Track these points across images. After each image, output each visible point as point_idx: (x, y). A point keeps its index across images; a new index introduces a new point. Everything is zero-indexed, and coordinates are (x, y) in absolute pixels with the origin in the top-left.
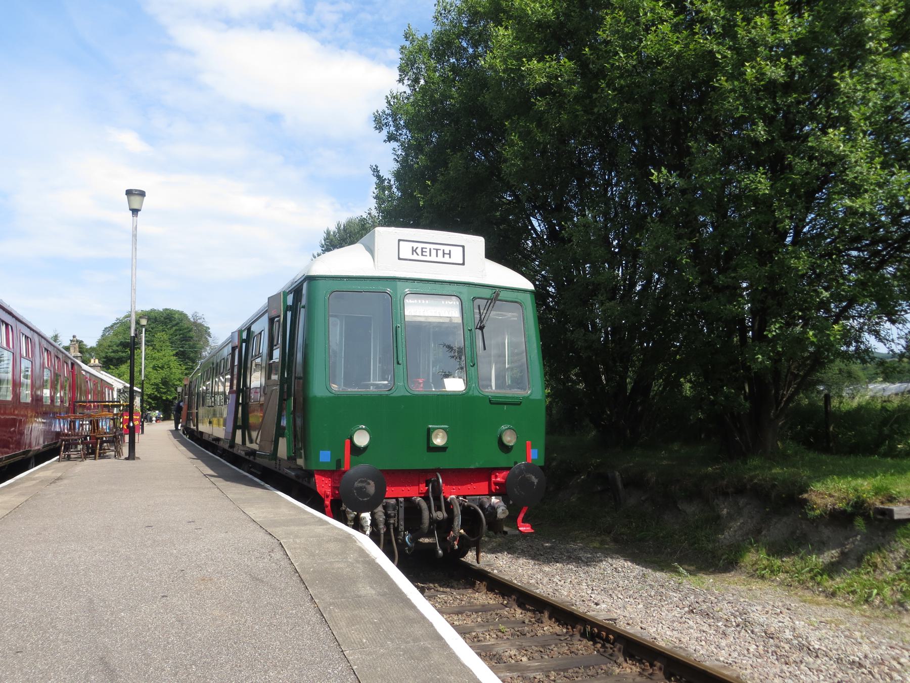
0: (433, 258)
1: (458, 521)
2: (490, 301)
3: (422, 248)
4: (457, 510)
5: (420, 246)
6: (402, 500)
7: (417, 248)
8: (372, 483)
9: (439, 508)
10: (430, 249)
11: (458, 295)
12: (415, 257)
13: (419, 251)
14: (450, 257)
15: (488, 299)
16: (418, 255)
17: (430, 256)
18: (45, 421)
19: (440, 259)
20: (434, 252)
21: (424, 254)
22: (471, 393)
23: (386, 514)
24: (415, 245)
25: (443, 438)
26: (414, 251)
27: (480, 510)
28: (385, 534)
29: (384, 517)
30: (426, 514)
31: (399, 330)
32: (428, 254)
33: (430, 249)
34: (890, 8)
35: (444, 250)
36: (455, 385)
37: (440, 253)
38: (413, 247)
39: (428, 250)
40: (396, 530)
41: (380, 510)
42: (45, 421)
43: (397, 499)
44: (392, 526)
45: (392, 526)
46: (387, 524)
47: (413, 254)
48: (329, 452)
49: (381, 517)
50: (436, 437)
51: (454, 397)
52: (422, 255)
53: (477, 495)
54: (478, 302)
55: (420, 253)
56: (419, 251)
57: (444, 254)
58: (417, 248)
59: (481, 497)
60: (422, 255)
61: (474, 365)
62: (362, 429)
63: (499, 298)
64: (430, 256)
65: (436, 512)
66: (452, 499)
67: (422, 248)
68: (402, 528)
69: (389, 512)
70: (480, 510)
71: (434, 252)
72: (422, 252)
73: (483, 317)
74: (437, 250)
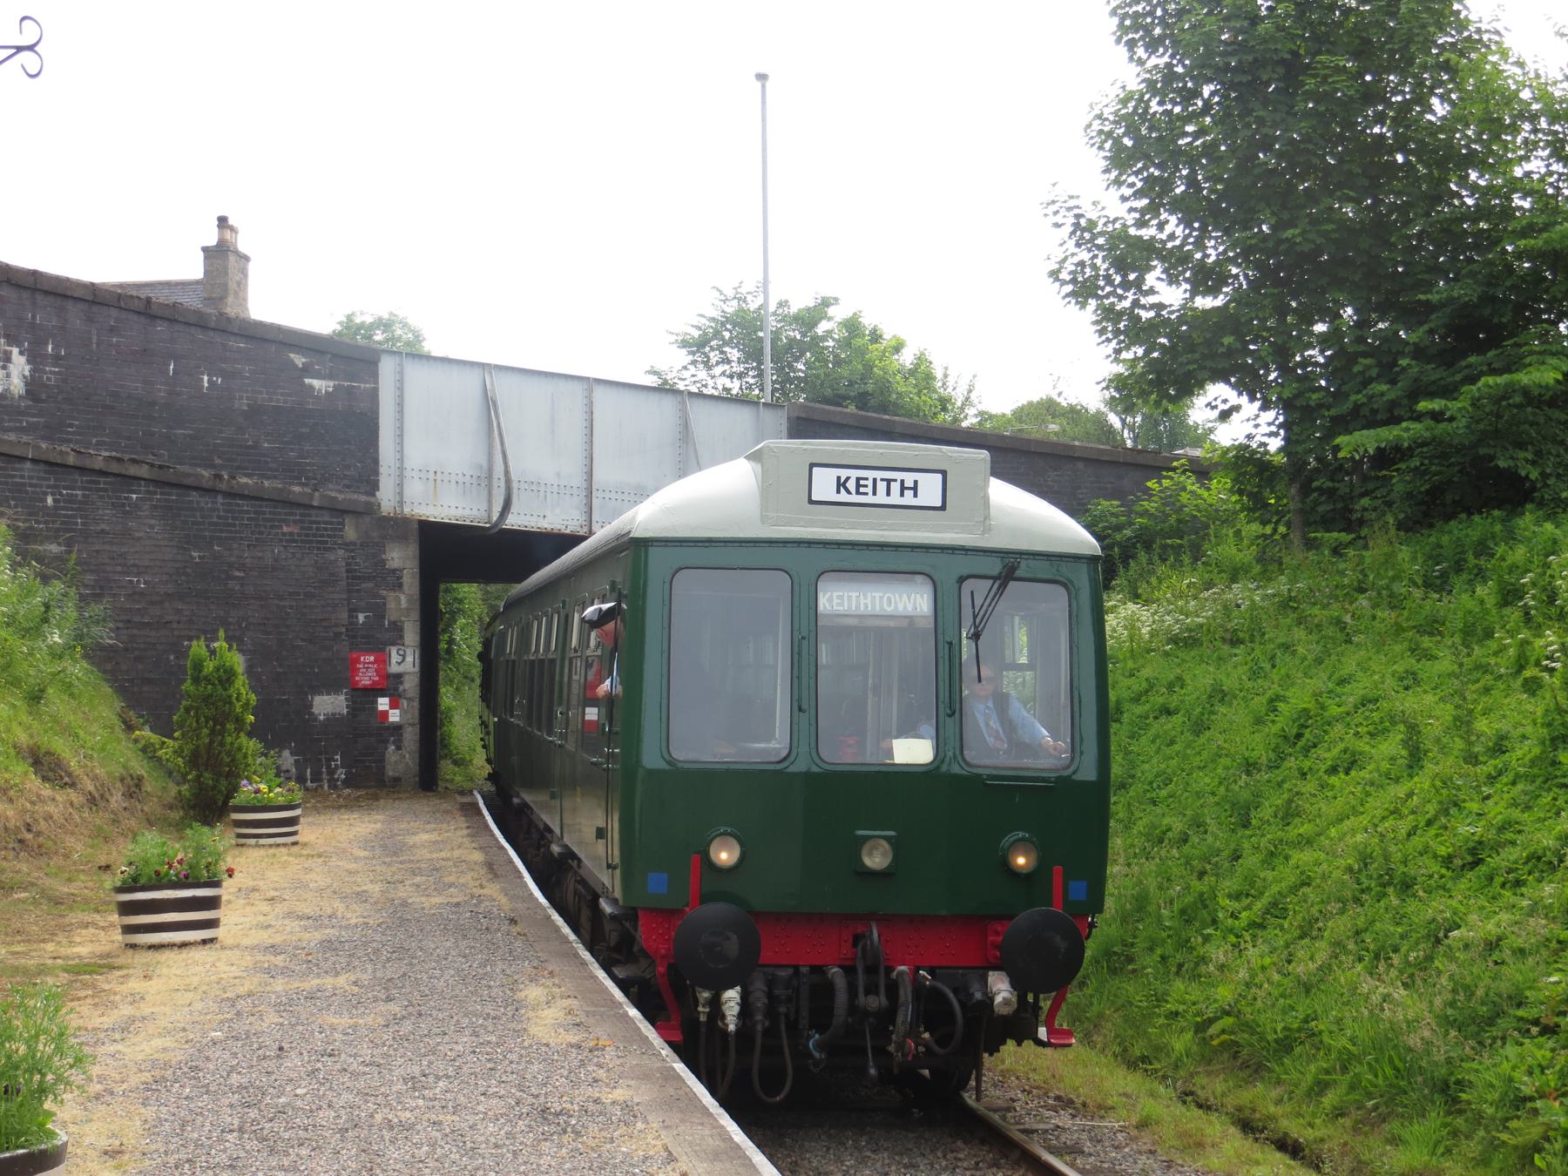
0: (881, 498)
1: (905, 1015)
2: (998, 583)
3: (858, 479)
4: (905, 994)
5: (855, 474)
6: (804, 970)
7: (848, 478)
8: (734, 938)
9: (871, 990)
10: (875, 480)
11: (927, 570)
12: (843, 497)
13: (851, 485)
14: (915, 495)
15: (995, 578)
16: (849, 492)
17: (874, 493)
18: (1385, 399)
19: (895, 498)
20: (882, 486)
21: (862, 490)
22: (944, 768)
23: (770, 995)
24: (844, 473)
25: (884, 854)
26: (841, 485)
27: (951, 996)
28: (766, 1032)
29: (766, 1001)
30: (841, 998)
31: (805, 643)
32: (869, 490)
33: (875, 480)
34: (49, 647)
35: (902, 482)
36: (913, 751)
37: (896, 487)
38: (839, 478)
39: (870, 483)
40: (793, 1026)
41: (759, 985)
42: (1385, 399)
43: (796, 968)
44: (783, 1019)
45: (783, 1019)
46: (771, 1012)
47: (838, 491)
48: (666, 875)
49: (760, 1001)
50: (870, 854)
51: (909, 775)
52: (858, 492)
53: (959, 968)
54: (968, 586)
55: (853, 490)
56: (851, 485)
57: (903, 488)
58: (848, 478)
59: (967, 971)
60: (858, 492)
61: (954, 713)
62: (725, 834)
63: (1018, 573)
64: (874, 493)
65: (866, 995)
66: (901, 974)
67: (858, 479)
68: (804, 1023)
69: (776, 992)
70: (951, 996)
71: (882, 486)
72: (858, 486)
73: (978, 621)
74: (889, 481)
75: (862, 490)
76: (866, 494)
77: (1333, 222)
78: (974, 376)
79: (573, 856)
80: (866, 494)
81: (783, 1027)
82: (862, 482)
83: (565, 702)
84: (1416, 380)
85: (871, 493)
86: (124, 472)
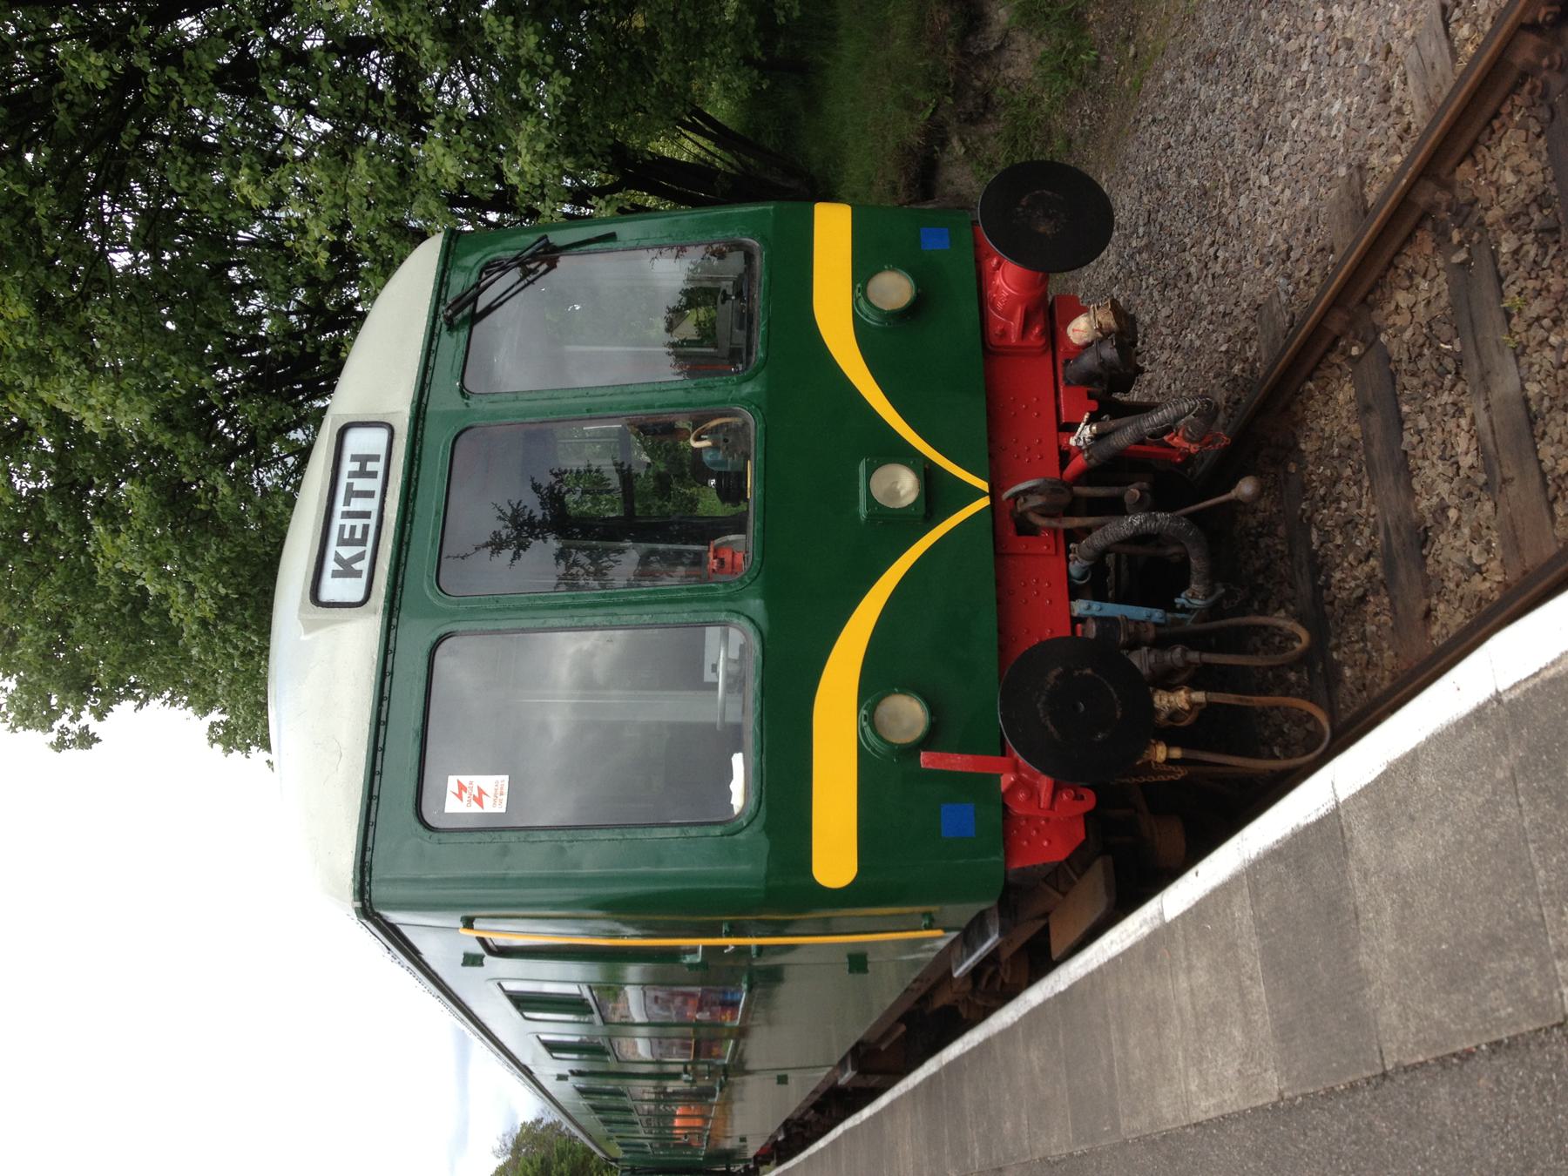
20: (358, 505)
24: (331, 565)
26: (346, 570)
37: (360, 484)
39: (349, 522)
52: (363, 542)
55: (356, 550)
60: (363, 542)
75: (358, 535)
76: (366, 528)
77: (505, 269)
78: (532, 479)
79: (854, 1051)
80: (366, 528)
81: (1215, 624)
82: (346, 536)
83: (610, 1084)
84: (1171, 1079)
85: (365, 521)
86: (663, 1029)
